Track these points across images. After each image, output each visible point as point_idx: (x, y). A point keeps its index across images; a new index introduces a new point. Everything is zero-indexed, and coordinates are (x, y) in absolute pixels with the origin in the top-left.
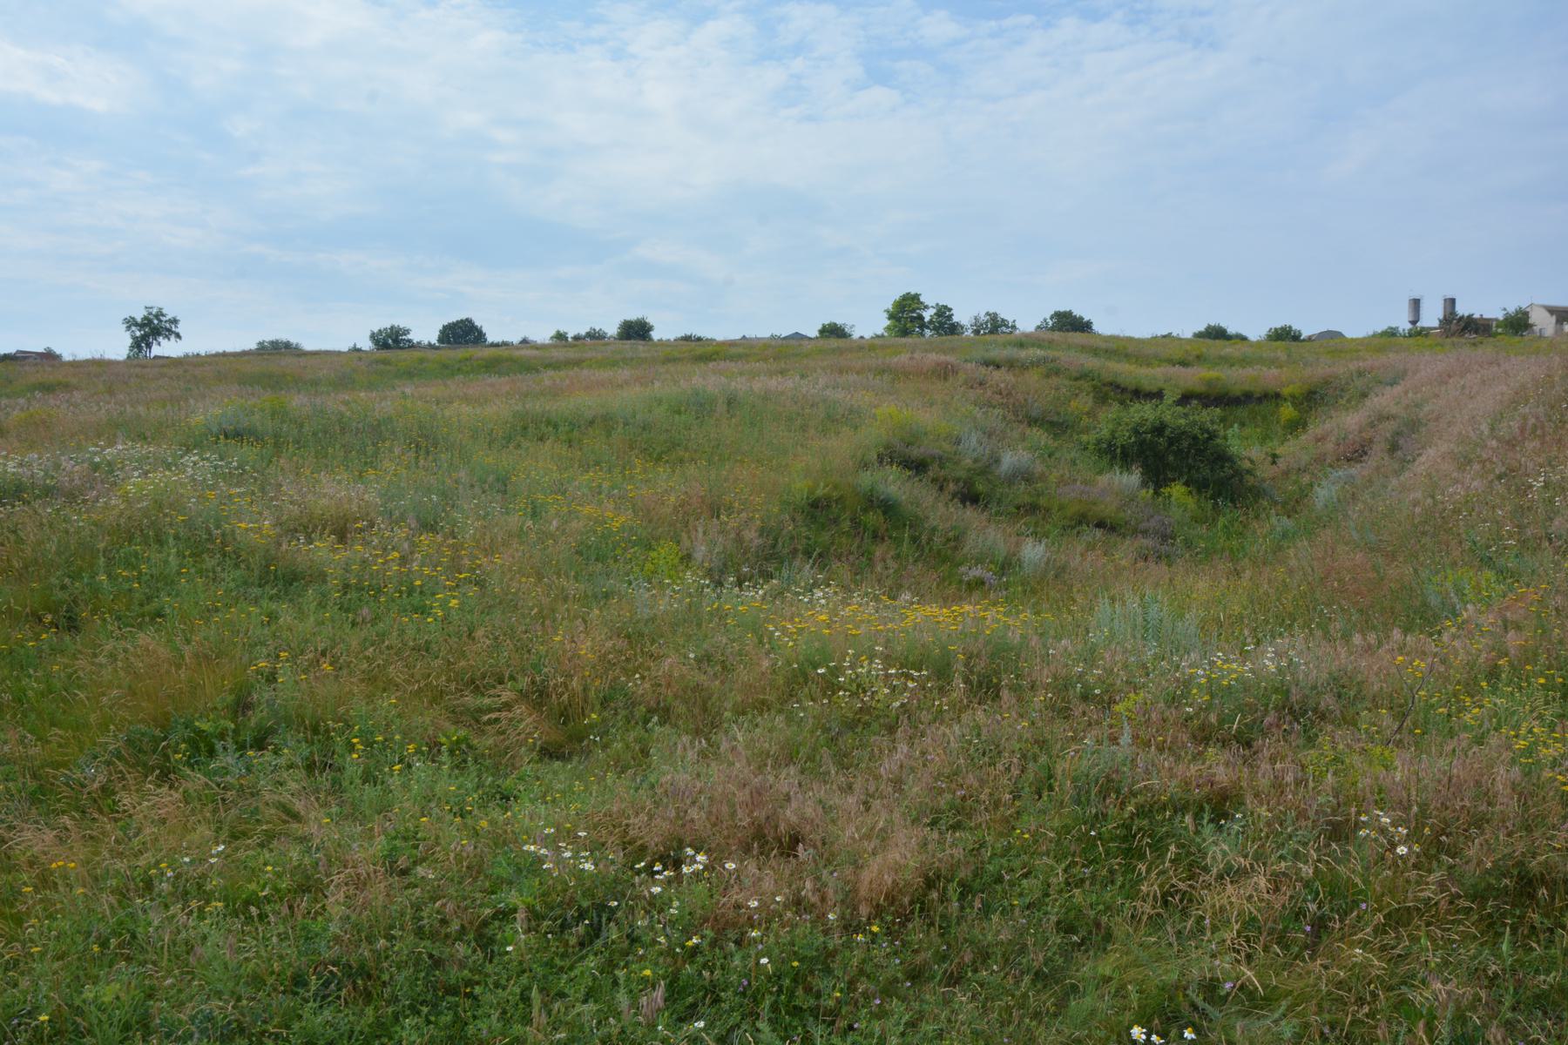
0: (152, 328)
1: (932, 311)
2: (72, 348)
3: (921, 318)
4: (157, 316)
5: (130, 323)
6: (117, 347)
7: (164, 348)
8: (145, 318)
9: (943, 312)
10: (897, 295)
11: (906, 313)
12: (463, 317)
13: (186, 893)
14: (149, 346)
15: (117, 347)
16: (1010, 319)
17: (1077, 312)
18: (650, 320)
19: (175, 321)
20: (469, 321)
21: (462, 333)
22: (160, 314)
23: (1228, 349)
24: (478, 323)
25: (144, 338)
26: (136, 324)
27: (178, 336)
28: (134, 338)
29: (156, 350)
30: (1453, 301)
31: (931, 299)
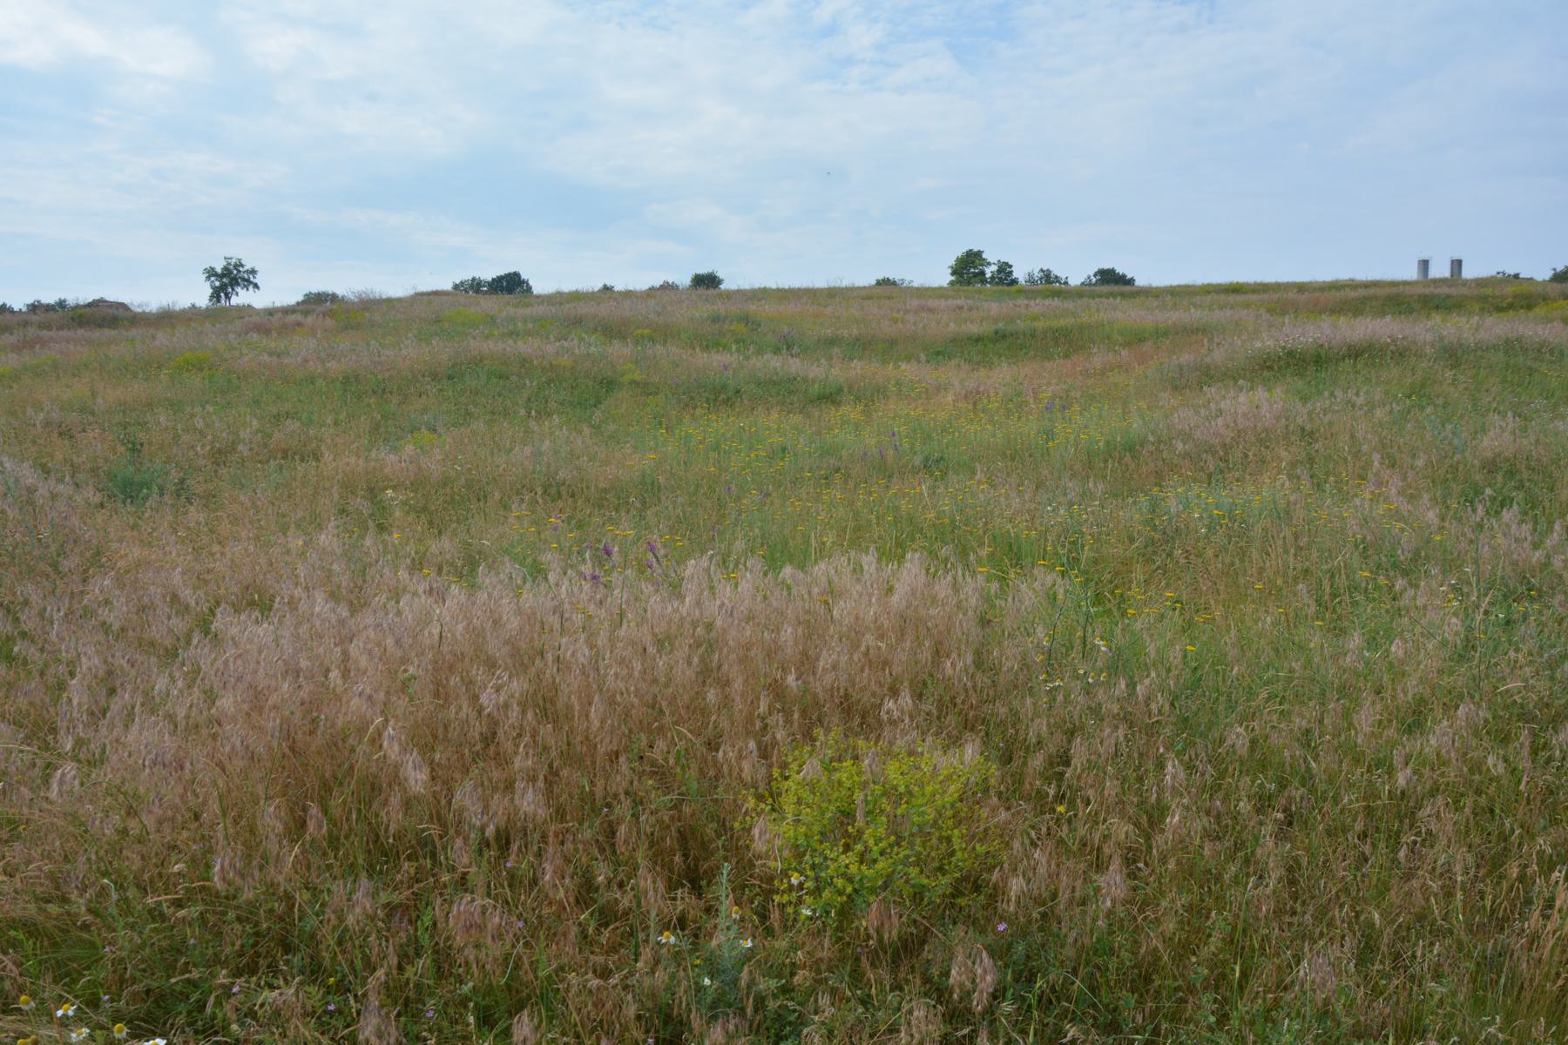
0: (230, 278)
1: (994, 268)
2: (146, 296)
3: (983, 273)
4: (236, 266)
5: (211, 273)
6: (199, 295)
7: (241, 297)
8: (225, 268)
9: (1005, 269)
10: (960, 251)
11: (968, 267)
12: (512, 270)
13: (973, 837)
14: (228, 297)
15: (199, 295)
16: (1062, 276)
17: (1120, 270)
18: (720, 275)
19: (253, 272)
20: (516, 275)
21: (1048, 277)
22: (239, 265)
23: (1125, 314)
24: (523, 276)
25: (223, 288)
26: (216, 275)
27: (256, 286)
28: (214, 288)
29: (235, 301)
30: (1459, 262)
31: (993, 256)
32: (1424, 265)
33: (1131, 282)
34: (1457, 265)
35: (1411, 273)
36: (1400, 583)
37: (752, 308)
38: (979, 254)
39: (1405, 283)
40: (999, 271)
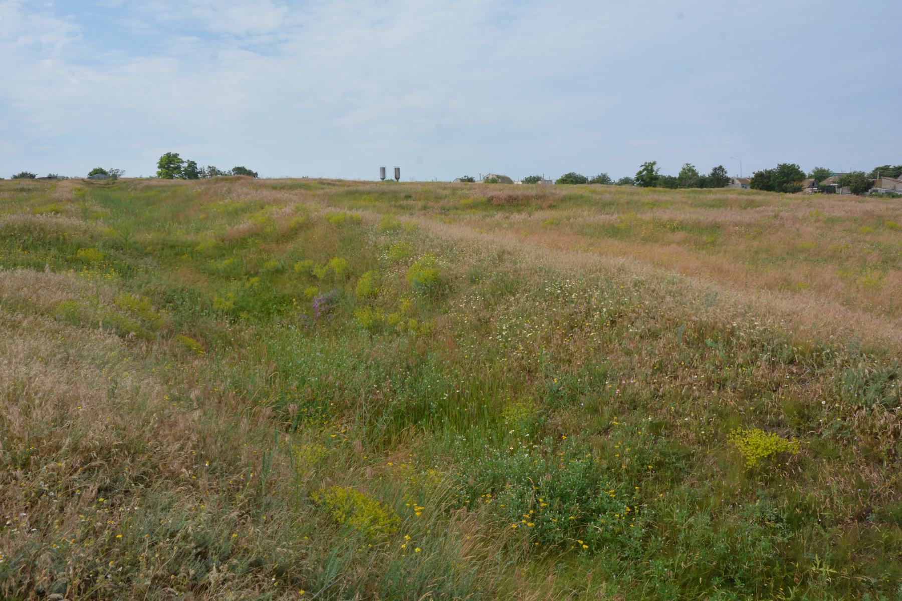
1: (186, 165)
3: (179, 168)
9: (192, 165)
10: (162, 153)
11: (169, 164)
17: (248, 168)
31: (185, 156)
32: (383, 170)
33: (255, 175)
34: (397, 171)
35: (377, 178)
36: (114, 450)
37: (371, 215)
38: (176, 156)
39: (372, 183)
40: (189, 166)
